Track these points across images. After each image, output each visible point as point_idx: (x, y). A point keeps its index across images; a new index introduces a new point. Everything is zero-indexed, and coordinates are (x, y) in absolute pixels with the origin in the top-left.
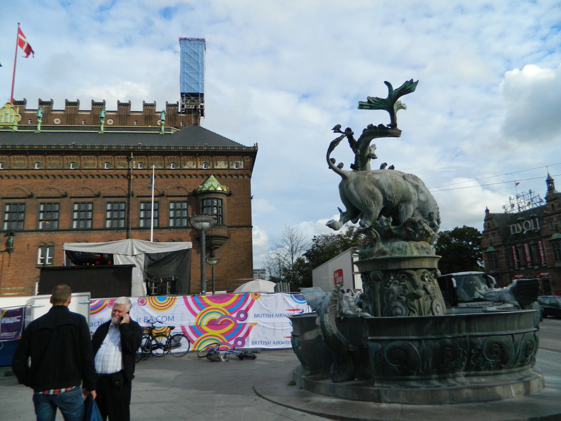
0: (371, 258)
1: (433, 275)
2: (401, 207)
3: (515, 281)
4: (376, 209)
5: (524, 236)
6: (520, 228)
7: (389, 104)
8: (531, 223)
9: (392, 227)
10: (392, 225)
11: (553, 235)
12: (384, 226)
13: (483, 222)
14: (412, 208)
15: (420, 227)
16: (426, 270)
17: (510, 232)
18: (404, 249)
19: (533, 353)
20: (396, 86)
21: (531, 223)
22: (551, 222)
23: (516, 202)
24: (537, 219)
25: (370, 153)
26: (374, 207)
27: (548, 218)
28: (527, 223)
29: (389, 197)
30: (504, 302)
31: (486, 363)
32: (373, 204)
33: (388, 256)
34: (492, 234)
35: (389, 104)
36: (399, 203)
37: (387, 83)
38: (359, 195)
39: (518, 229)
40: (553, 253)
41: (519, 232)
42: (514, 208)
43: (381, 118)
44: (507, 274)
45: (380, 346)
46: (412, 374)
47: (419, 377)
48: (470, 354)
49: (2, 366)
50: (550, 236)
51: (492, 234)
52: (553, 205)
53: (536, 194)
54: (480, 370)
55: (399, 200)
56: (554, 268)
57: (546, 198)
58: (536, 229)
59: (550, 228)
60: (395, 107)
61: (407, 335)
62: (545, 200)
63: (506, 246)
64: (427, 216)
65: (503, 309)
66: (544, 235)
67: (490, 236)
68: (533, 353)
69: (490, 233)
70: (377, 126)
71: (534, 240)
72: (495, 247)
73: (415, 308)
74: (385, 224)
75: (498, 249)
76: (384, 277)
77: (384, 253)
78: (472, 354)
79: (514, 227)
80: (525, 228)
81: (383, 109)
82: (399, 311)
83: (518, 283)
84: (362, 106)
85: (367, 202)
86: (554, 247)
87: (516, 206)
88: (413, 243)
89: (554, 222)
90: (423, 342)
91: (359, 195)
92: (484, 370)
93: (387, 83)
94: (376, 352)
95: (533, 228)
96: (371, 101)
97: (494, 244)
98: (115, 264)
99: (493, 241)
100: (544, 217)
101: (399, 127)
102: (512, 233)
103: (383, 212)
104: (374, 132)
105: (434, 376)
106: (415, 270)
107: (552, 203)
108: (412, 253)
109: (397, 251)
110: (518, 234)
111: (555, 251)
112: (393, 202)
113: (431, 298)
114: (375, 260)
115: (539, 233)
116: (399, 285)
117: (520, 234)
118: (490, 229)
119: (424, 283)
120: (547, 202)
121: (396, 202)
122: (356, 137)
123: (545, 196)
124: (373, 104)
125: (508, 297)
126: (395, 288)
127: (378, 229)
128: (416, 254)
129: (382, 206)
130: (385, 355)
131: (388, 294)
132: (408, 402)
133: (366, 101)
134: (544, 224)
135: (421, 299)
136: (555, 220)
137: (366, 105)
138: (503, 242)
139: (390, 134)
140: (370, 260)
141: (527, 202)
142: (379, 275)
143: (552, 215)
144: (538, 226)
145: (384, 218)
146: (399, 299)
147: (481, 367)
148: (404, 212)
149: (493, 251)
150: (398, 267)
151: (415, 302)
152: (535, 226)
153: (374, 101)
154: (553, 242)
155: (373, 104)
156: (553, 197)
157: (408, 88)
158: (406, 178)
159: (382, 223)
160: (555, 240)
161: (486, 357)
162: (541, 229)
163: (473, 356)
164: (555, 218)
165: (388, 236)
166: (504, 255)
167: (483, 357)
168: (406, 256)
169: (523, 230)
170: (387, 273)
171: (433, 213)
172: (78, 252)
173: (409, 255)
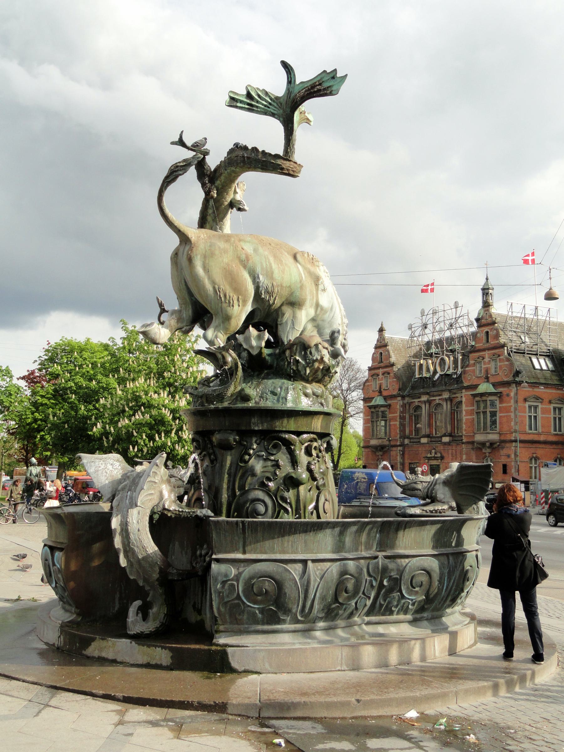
0: (220, 406)
1: (325, 446)
2: (283, 314)
3: (455, 465)
4: (240, 312)
5: (434, 384)
6: (432, 368)
7: (286, 109)
9: (266, 351)
10: (266, 347)
11: (480, 387)
12: (252, 347)
13: (373, 350)
14: (304, 316)
15: (317, 356)
16: (315, 436)
17: (414, 373)
18: (283, 394)
19: (471, 585)
20: (304, 75)
23: (430, 321)
25: (234, 199)
26: (236, 307)
27: (477, 354)
29: (267, 292)
30: (434, 500)
31: (403, 601)
32: (236, 302)
33: (251, 404)
34: (383, 374)
35: (286, 109)
36: (282, 305)
37: (285, 65)
38: (213, 283)
39: (428, 370)
40: (475, 417)
41: (428, 376)
42: (427, 331)
43: (265, 134)
44: (399, 448)
45: (233, 571)
46: (284, 622)
47: (299, 626)
48: (381, 586)
49: (1, 694)
50: (475, 387)
51: (383, 374)
52: (381, 353)
53: (464, 311)
54: (391, 613)
55: (283, 300)
56: (473, 443)
57: (478, 320)
58: (456, 373)
60: (297, 116)
61: (284, 552)
62: (475, 324)
63: (403, 397)
64: (328, 338)
65: (431, 512)
67: (381, 376)
68: (471, 585)
69: (381, 371)
70: (260, 150)
71: (450, 391)
72: (385, 398)
73: (290, 504)
74: (254, 343)
75: (389, 402)
76: (239, 443)
77: (246, 398)
78: (384, 586)
80: (438, 369)
81: (273, 115)
82: (261, 508)
83: (462, 469)
84: (233, 102)
85: (225, 296)
86: (478, 407)
87: (430, 327)
88: (300, 385)
89: (485, 364)
90: (310, 564)
91: (213, 283)
92: (398, 613)
93: (285, 65)
94: (224, 583)
95: (451, 371)
96: (253, 94)
97: (385, 393)
99: (384, 387)
100: (471, 352)
101: (298, 156)
102: (417, 376)
103: (250, 320)
104: (246, 159)
105: (321, 624)
106: (298, 434)
107: (381, 350)
108: (296, 400)
109: (270, 396)
110: (426, 378)
111: (478, 413)
112: (271, 302)
113: (318, 488)
114: (227, 411)
115: (459, 380)
116: (266, 460)
117: (429, 378)
118: (382, 364)
119: (310, 459)
120: (479, 327)
121: (278, 303)
122: (212, 162)
123: (476, 316)
124: (250, 102)
125: (442, 492)
126: (258, 466)
127: (238, 348)
128: (305, 404)
129: (249, 308)
130: (241, 589)
131: (244, 477)
132: (272, 670)
133: (245, 93)
134: (468, 366)
135: (302, 488)
136: (487, 360)
137: (241, 102)
138: (399, 390)
139: (282, 169)
140: (217, 410)
141: (448, 323)
142: (231, 439)
143: (484, 350)
144: (459, 367)
145: (252, 331)
146: (263, 486)
147: (393, 609)
148: (290, 323)
149: (382, 406)
150: (270, 428)
151: (290, 495)
153: (259, 96)
154: (478, 399)
155: (250, 102)
157: (325, 85)
158: (299, 257)
159: (248, 340)
160: (482, 395)
161: (404, 592)
162: (464, 372)
163: (383, 591)
165: (256, 367)
166: (398, 414)
167: (400, 591)
168: (284, 407)
169: (435, 372)
170: (246, 434)
171: (339, 332)
173: (290, 405)
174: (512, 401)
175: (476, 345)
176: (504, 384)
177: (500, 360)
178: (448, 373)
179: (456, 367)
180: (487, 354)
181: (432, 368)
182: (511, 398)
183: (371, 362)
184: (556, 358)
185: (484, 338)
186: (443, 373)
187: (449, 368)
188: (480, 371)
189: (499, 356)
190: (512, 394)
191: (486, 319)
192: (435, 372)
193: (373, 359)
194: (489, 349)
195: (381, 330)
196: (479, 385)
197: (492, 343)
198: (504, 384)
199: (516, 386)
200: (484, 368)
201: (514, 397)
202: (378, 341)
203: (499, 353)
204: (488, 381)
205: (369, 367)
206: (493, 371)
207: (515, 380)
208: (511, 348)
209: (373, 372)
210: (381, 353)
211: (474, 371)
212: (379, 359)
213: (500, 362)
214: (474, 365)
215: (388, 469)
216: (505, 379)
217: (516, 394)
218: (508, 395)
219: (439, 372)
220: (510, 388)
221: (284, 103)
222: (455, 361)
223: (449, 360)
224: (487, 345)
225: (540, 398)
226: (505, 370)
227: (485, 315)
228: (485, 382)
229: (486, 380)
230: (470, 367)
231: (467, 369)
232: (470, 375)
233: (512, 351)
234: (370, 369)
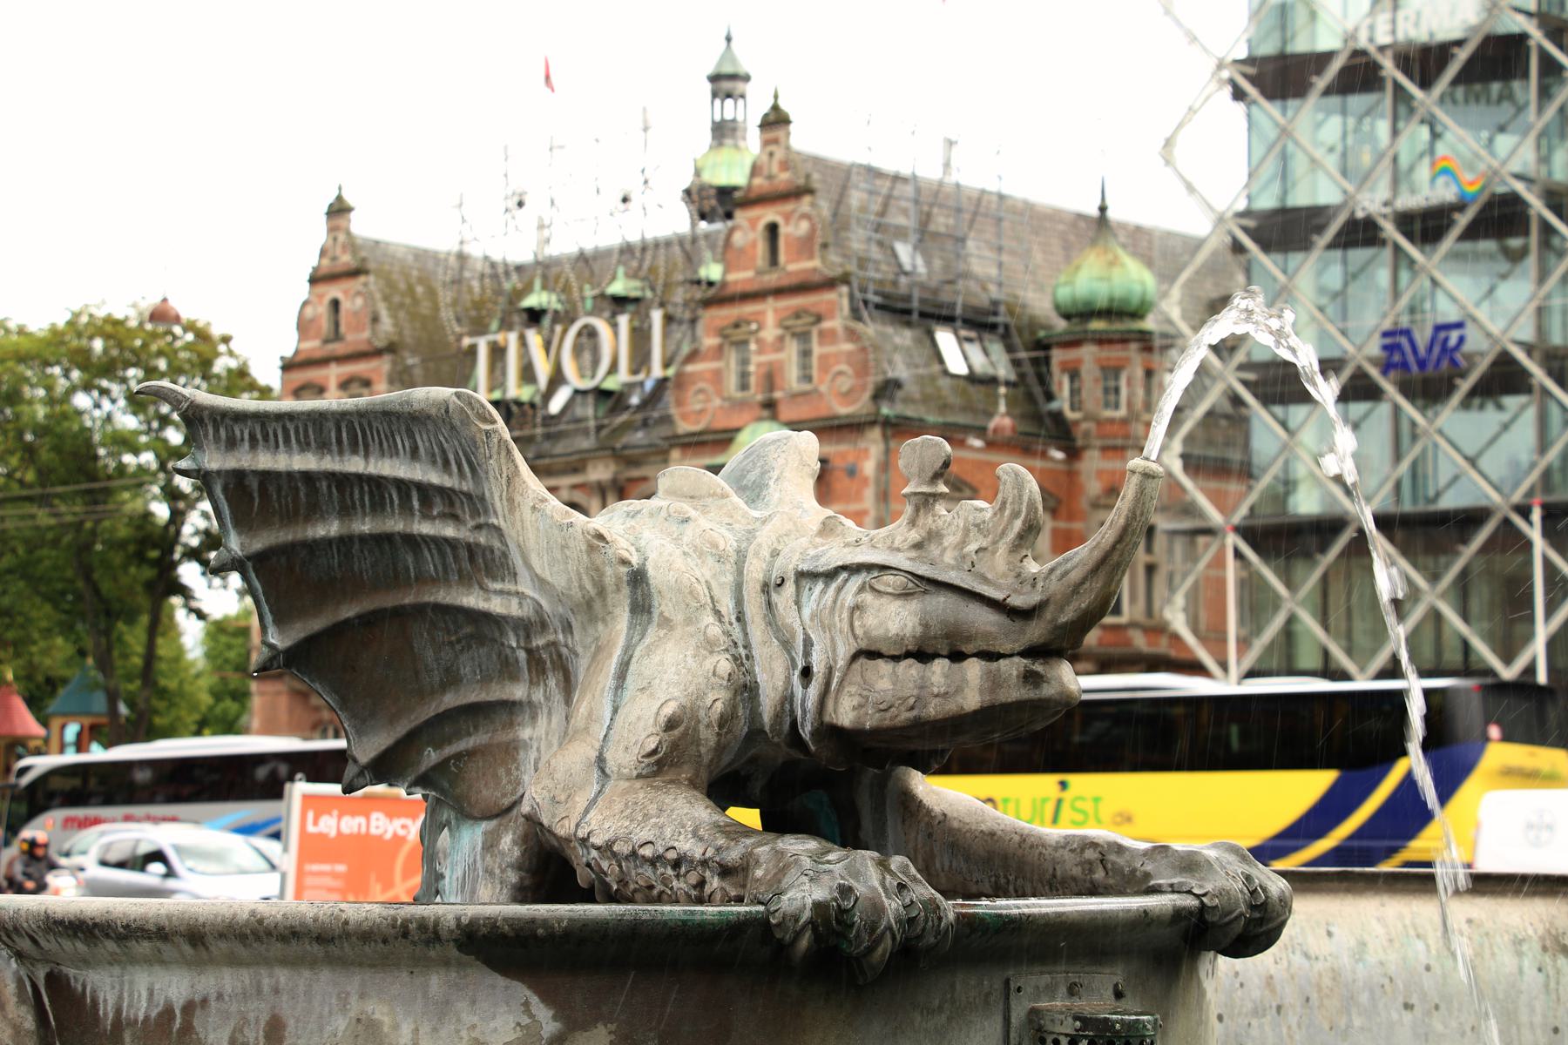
6: (543, 370)
8: (614, 338)
16: (983, 619)
21: (614, 338)
22: (742, 344)
24: (657, 316)
28: (590, 333)
39: (527, 374)
41: (525, 393)
52: (335, 304)
59: (732, 381)
66: (684, 427)
79: (498, 352)
95: (624, 376)
98: (757, 811)
107: (334, 291)
118: (338, 348)
134: (693, 356)
152: (640, 358)
156: (346, 259)
164: (770, 319)
172: (215, 733)
174: (869, 494)
175: (731, 277)
176: (840, 428)
177: (821, 334)
178: (611, 384)
179: (640, 358)
180: (770, 314)
181: (543, 370)
182: (865, 481)
183: (295, 335)
184: (1020, 330)
185: (761, 248)
186: (587, 384)
187: (613, 369)
188: (744, 375)
189: (819, 319)
190: (869, 467)
191: (770, 177)
192: (557, 379)
193: (304, 327)
194: (779, 292)
195: (339, 210)
196: (738, 430)
197: (792, 267)
198: (840, 428)
199: (885, 438)
200: (759, 365)
201: (878, 481)
202: (323, 253)
203: (822, 309)
204: (774, 417)
205: (204, 574)
206: (792, 377)
207: (877, 413)
208: (863, 290)
209: (301, 377)
210: (335, 304)
211: (717, 377)
212: (325, 324)
213: (821, 343)
214: (719, 352)
215: (1382, 675)
216: (843, 410)
217: (885, 466)
218: (852, 472)
219: (575, 380)
220: (862, 444)
221: (65, 407)
222: (640, 337)
223: (616, 334)
224: (772, 279)
225: (965, 483)
226: (840, 373)
227: (765, 158)
228: (760, 419)
229: (766, 413)
230: (704, 359)
231: (690, 368)
232: (701, 391)
233: (866, 302)
234: (288, 366)
